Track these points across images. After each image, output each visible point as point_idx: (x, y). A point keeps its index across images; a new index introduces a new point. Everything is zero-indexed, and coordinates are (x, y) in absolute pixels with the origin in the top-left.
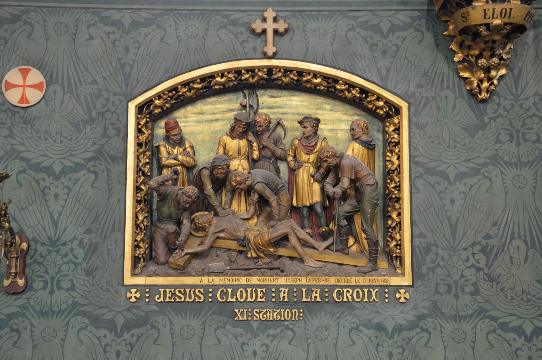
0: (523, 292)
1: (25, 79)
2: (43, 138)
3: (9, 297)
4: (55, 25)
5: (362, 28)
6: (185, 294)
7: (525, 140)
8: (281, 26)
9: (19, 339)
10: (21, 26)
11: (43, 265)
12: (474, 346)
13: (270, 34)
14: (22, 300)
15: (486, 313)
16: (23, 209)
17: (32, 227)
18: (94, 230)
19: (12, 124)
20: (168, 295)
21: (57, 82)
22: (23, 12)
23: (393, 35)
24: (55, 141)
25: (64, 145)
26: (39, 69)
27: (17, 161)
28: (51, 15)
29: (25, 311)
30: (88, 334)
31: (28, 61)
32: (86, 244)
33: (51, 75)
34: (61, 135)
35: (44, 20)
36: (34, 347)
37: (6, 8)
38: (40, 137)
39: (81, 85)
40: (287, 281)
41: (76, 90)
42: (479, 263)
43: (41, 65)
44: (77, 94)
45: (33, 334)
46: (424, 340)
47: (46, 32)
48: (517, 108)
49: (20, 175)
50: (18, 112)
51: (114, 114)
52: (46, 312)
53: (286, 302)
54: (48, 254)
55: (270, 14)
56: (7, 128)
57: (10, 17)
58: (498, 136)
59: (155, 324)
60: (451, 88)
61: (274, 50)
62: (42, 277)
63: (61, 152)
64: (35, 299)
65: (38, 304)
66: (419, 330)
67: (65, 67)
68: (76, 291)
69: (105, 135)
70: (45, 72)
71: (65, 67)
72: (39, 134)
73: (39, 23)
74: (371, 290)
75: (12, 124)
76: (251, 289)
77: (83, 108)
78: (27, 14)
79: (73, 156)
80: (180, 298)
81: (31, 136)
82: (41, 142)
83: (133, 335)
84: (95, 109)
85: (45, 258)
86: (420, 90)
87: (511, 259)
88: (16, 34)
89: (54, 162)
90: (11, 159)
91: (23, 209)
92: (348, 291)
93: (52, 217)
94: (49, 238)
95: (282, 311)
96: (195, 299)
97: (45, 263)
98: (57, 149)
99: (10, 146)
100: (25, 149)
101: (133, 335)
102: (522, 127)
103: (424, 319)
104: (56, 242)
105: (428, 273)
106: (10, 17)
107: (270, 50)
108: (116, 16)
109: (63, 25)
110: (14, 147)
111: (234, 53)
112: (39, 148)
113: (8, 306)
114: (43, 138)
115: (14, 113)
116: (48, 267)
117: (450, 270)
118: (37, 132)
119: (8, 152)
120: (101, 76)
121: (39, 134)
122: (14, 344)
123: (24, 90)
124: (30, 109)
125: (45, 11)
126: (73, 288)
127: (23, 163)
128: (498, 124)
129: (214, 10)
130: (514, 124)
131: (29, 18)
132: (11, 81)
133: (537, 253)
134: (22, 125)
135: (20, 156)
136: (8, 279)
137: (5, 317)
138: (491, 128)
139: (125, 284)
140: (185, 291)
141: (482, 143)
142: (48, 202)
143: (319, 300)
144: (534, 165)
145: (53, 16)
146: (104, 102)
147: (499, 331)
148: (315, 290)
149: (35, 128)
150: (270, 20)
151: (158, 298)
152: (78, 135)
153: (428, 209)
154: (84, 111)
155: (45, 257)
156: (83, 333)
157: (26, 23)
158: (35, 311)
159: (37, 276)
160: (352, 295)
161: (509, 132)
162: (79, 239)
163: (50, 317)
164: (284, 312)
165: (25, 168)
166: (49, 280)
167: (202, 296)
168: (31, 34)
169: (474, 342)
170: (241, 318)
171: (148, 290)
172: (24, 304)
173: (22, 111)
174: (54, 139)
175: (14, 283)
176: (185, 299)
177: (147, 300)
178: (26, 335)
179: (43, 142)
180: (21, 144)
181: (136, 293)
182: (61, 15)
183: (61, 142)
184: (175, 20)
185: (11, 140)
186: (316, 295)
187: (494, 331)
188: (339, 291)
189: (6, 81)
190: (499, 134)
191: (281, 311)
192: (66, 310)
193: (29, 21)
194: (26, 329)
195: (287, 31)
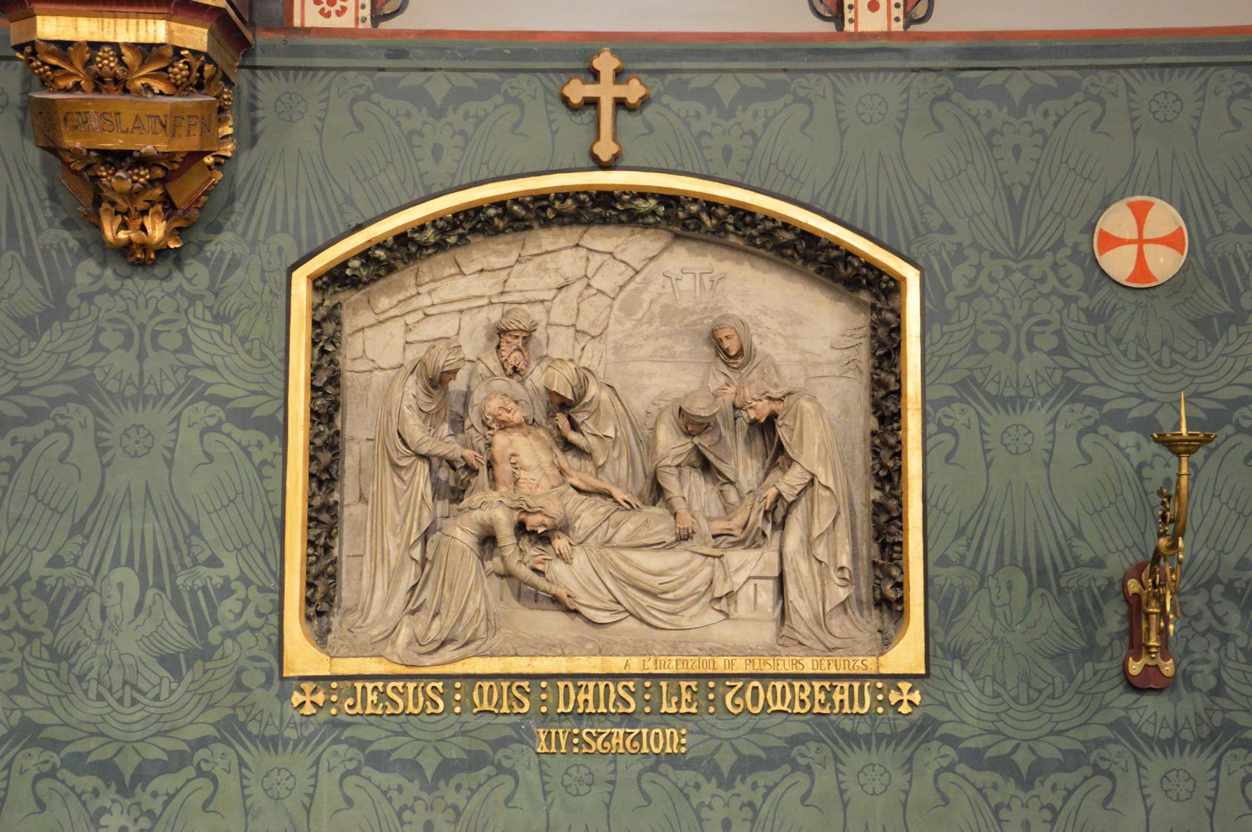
0: (125, 683)
7: (157, 347)
8: (633, 91)
12: (311, 803)
15: (934, 731)
17: (238, 550)
20: (372, 697)
23: (744, 110)
24: (1159, 362)
27: (202, 405)
30: (960, 781)
32: (53, 588)
38: (1124, 353)
39: (38, 230)
42: (31, 622)
46: (206, 794)
47: (841, 116)
48: (1017, 277)
51: (993, 299)
52: (273, 738)
59: (205, 767)
61: (614, 149)
66: (1088, 770)
72: (1122, 348)
75: (189, 322)
76: (414, 685)
77: (1220, 286)
81: (1105, 350)
83: (458, 787)
84: (951, 289)
87: (103, 610)
95: (645, 731)
96: (425, 708)
99: (184, 370)
100: (1092, 380)
102: (1026, 318)
103: (803, 743)
105: (1110, 644)
110: (1069, 374)
118: (1118, 342)
121: (247, 346)
127: (214, 409)
128: (976, 312)
130: (133, 311)
133: (1048, 594)
134: (1086, 328)
135: (206, 393)
141: (941, 353)
146: (971, 273)
147: (962, 768)
149: (240, 331)
151: (350, 707)
152: (1210, 349)
153: (230, 501)
154: (44, 292)
164: (648, 735)
165: (220, 419)
167: (526, 701)
169: (311, 796)
187: (950, 768)
190: (100, 330)
191: (640, 733)
195: (645, 101)
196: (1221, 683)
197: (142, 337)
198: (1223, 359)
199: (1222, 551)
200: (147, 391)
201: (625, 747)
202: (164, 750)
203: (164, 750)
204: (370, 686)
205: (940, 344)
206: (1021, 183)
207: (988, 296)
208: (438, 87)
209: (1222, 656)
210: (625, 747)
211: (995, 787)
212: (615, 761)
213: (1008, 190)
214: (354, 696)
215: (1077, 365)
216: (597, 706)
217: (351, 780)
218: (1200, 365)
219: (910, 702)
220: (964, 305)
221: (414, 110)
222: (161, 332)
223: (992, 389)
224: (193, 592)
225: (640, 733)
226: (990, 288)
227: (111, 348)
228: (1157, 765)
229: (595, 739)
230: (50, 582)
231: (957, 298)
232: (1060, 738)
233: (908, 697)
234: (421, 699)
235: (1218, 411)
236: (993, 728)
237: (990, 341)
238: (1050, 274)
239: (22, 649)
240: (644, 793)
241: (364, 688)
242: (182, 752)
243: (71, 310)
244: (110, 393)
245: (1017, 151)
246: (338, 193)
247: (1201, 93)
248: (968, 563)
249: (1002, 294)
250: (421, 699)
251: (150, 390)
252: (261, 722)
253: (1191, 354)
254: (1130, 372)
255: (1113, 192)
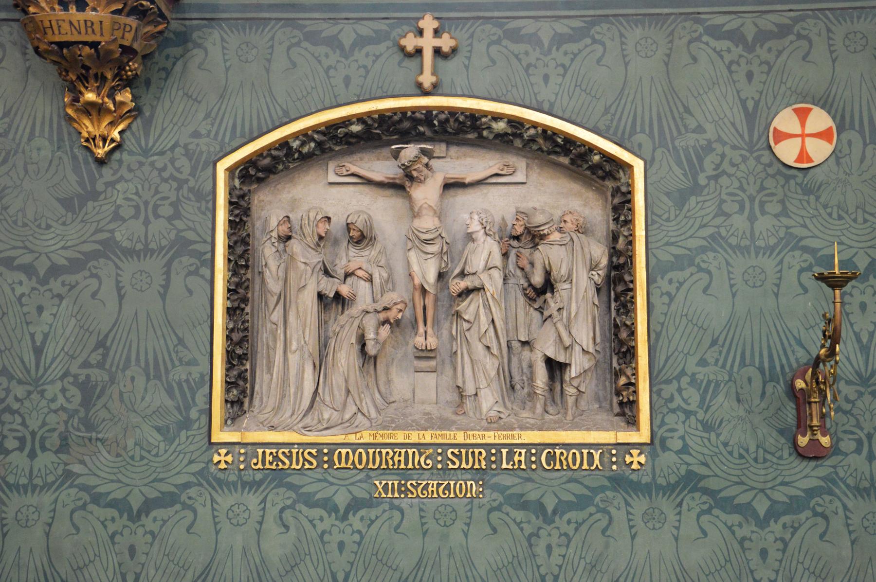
1: (803, 125)
2: (835, 215)
3: (805, 463)
4: (847, 37)
5: (712, 35)
6: (290, 457)
8: (446, 43)
9: (827, 528)
10: (792, 42)
11: (852, 415)
13: (428, 55)
14: (824, 469)
16: (811, 327)
18: (711, 361)
19: (785, 195)
20: (269, 458)
21: (852, 127)
22: (796, 20)
24: (855, 220)
25: (870, 227)
26: (822, 107)
27: (797, 253)
28: (839, 22)
29: (834, 488)
31: (805, 97)
32: (702, 381)
33: (843, 117)
34: (865, 211)
35: (829, 30)
36: (853, 542)
37: (770, 17)
38: (830, 215)
40: (520, 437)
41: (673, 143)
43: (826, 102)
44: (674, 148)
45: (850, 522)
47: (832, 48)
48: (752, 162)
49: (804, 274)
50: (794, 177)
52: (865, 489)
53: (523, 469)
54: (859, 397)
55: (428, 23)
56: (778, 202)
57: (776, 30)
58: (720, 206)
60: (647, 132)
61: (434, 79)
62: (853, 433)
63: (864, 238)
64: (846, 468)
65: (851, 475)
67: (864, 103)
68: (691, 455)
69: (721, 213)
70: (833, 111)
71: (864, 103)
72: (829, 210)
73: (820, 35)
74: (592, 451)
75: (785, 195)
77: (683, 169)
78: (801, 23)
79: (672, 244)
80: (454, 463)
81: (816, 213)
82: (831, 221)
83: (155, 520)
85: (854, 405)
86: (196, 141)
88: (784, 56)
89: (856, 253)
90: (787, 250)
91: (811, 327)
92: (562, 453)
93: (859, 340)
94: (856, 372)
95: (452, 483)
97: (855, 411)
98: (860, 232)
99: (784, 229)
101: (566, 54)
104: (869, 379)
105: (199, 418)
106: (776, 30)
107: (427, 79)
108: (529, 27)
109: (859, 36)
110: (791, 230)
111: (715, 80)
112: (830, 232)
113: (805, 477)
114: (835, 215)
115: (788, 178)
116: (861, 419)
117: (858, 417)
118: (825, 207)
119: (782, 239)
120: (710, 119)
121: (829, 210)
122: (822, 536)
123: (803, 142)
124: (811, 170)
125: (831, 16)
126: (685, 450)
127: (806, 256)
128: (721, 187)
129: (681, 14)
130: (745, 186)
131: (805, 29)
132: (780, 128)
134: (801, 197)
135: (800, 244)
136: (804, 435)
137: (803, 495)
138: (105, 199)
139: (649, 442)
140: (290, 452)
141: (696, 215)
142: (850, 316)
143: (523, 466)
144: (777, 251)
145: (843, 22)
148: (519, 450)
149: (822, 200)
150: (428, 33)
154: (685, 175)
155: (853, 402)
156: (495, 515)
157: (799, 36)
158: (848, 486)
159: (845, 432)
160: (566, 459)
161: (135, 203)
162: (690, 373)
163: (29, 494)
165: (811, 263)
166: (29, 438)
168: (808, 54)
170: (384, 495)
171: (242, 451)
172: (829, 475)
173: (800, 175)
174: (853, 217)
175: (814, 442)
176: (460, 465)
177: (326, 466)
178: (837, 523)
179: (837, 222)
180: (802, 226)
181: (219, 454)
182: (855, 20)
183: (865, 221)
184: (619, 31)
185: (785, 221)
186: (520, 456)
188: (549, 452)
189: (775, 129)
190: (723, 201)
191: (449, 484)
192: (54, 483)
193: (804, 33)
194: (837, 514)
195: (454, 50)
196: (686, 446)
197: (146, 211)
198: (687, 220)
199: (688, 353)
200: (150, 247)
201: (438, 494)
202: (574, 494)
203: (574, 494)
204: (268, 451)
205: (697, 209)
206: (753, 98)
207: (729, 176)
208: (348, 34)
209: (687, 427)
210: (438, 494)
211: (321, 519)
212: (472, 502)
213: (743, 102)
214: (257, 457)
215: (710, 224)
216: (406, 464)
217: (705, 518)
218: (673, 223)
219: (226, 462)
220: (712, 182)
221: (733, 48)
222: (767, 202)
223: (733, 241)
224: (179, 384)
225: (449, 484)
226: (731, 170)
227: (127, 218)
228: (640, 505)
229: (416, 488)
230: (700, 377)
231: (707, 177)
232: (787, 488)
233: (637, 458)
234: (301, 459)
235: (78, 259)
236: (115, 478)
237: (731, 207)
238: (169, 165)
239: (684, 423)
240: (74, 525)
241: (264, 453)
242: (171, 494)
243: (100, 193)
244: (730, 245)
245: (546, 78)
246: (679, 105)
247: (671, 38)
248: (720, 363)
249: (739, 174)
250: (301, 459)
251: (153, 246)
252: (51, 472)
253: (665, 217)
254: (835, 228)
255: (611, 105)
